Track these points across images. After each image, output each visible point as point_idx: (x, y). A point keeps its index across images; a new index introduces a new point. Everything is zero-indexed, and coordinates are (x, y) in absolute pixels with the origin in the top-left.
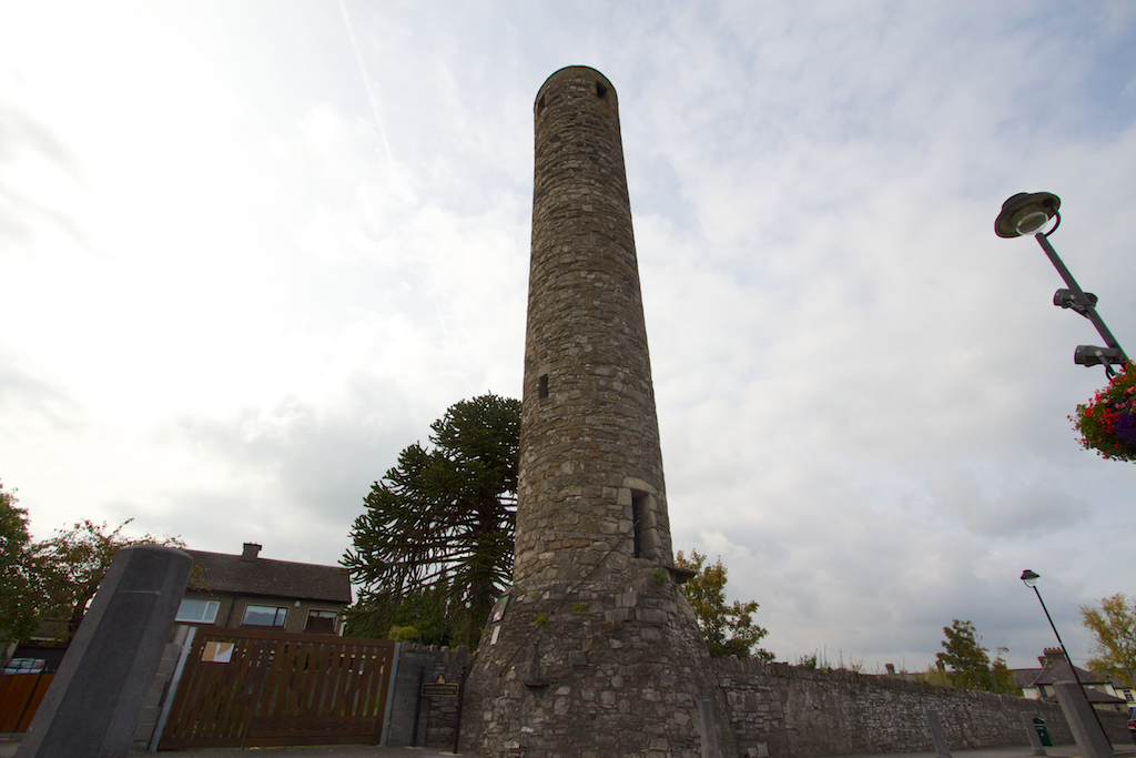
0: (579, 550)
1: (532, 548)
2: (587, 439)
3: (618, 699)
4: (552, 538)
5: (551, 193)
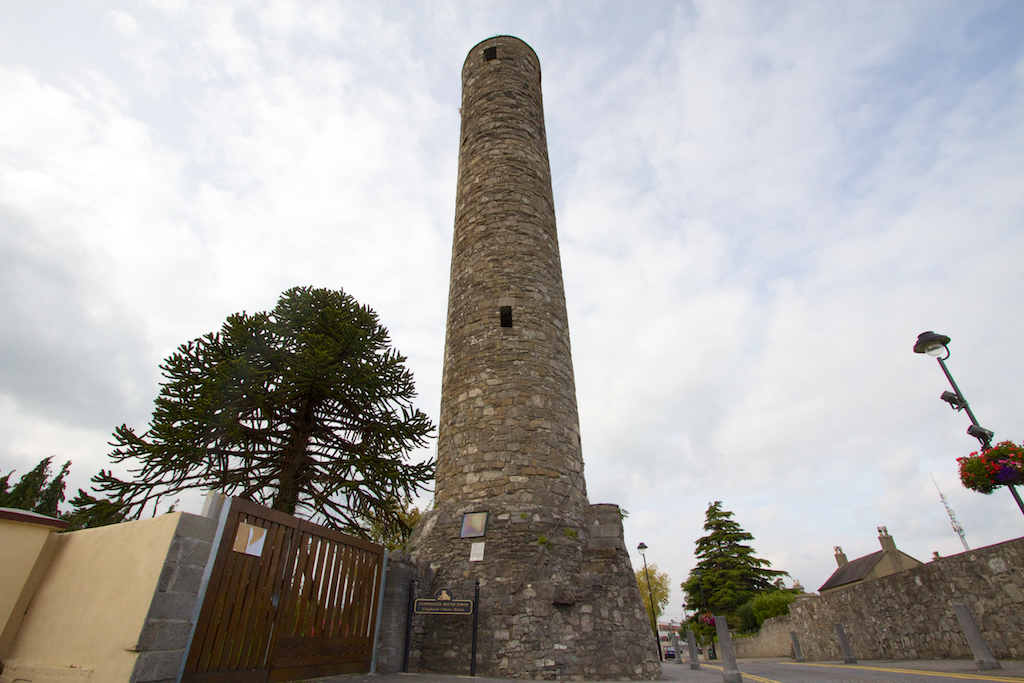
0: (551, 479)
1: (500, 469)
2: (552, 379)
3: (623, 616)
4: (526, 463)
5: (507, 141)
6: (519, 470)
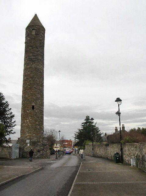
6: (34, 134)
